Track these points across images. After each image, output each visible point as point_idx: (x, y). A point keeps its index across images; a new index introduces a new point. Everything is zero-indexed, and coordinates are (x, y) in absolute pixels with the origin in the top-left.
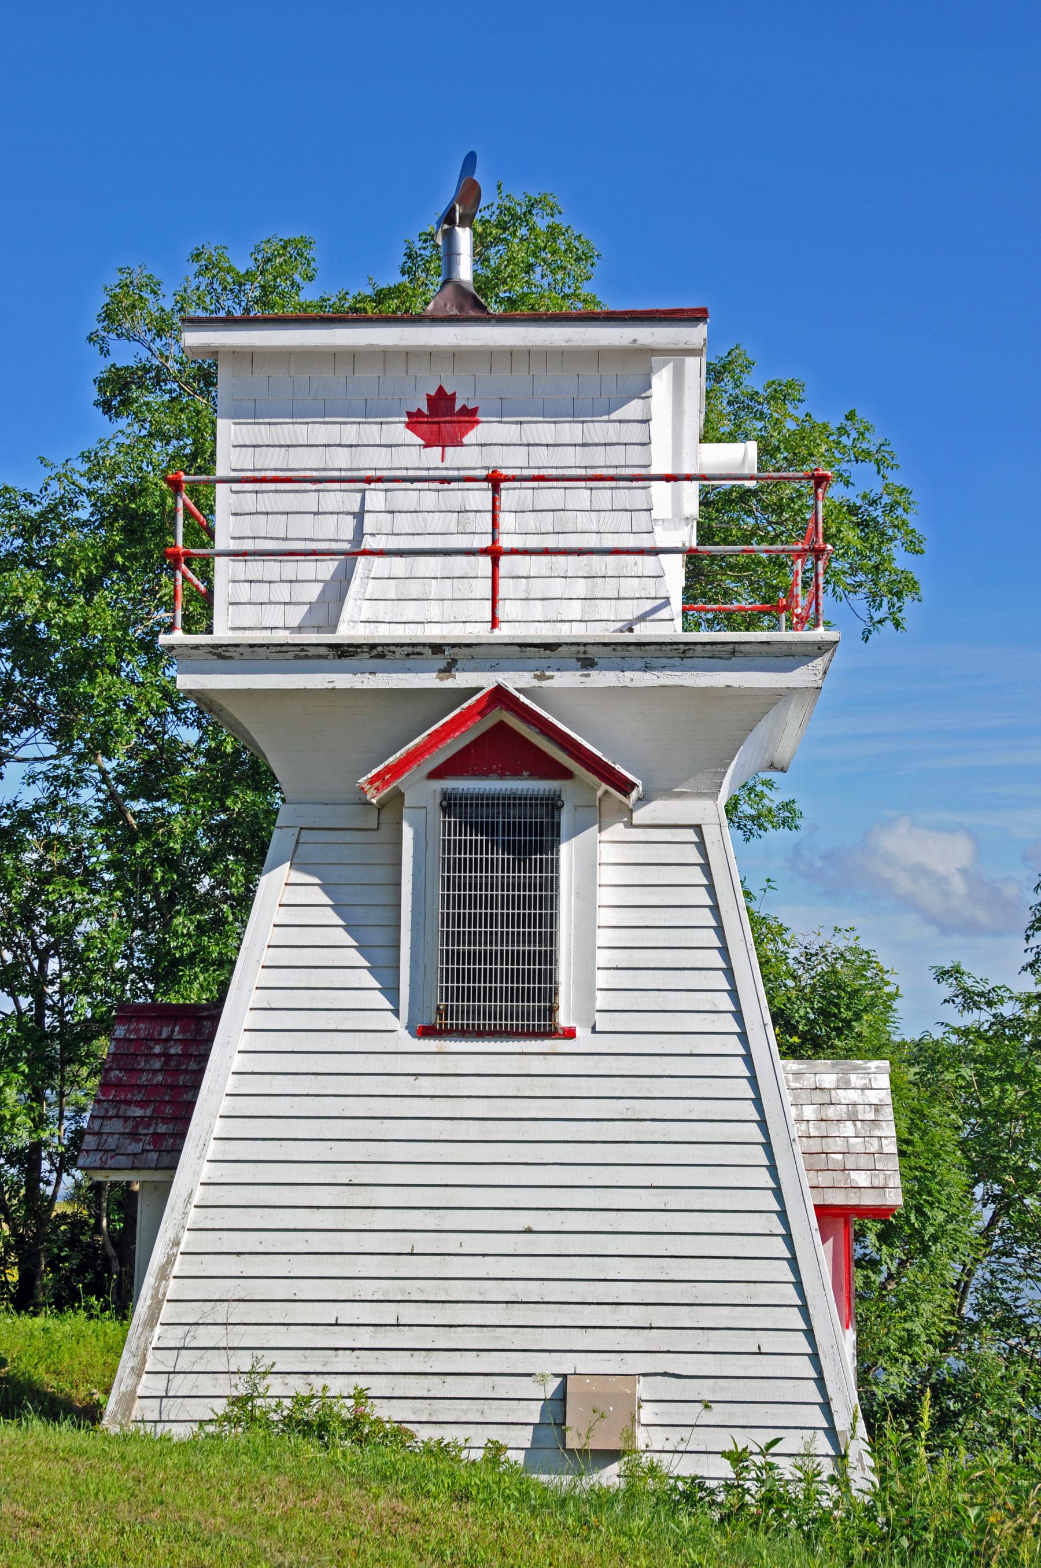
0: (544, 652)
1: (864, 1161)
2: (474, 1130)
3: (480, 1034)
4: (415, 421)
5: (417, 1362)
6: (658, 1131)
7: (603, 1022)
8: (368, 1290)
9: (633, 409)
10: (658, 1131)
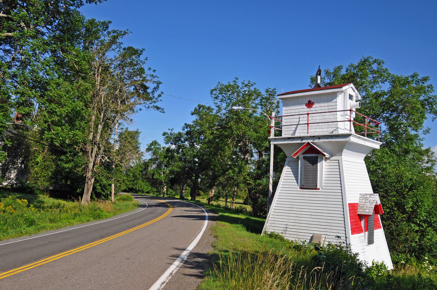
1: (368, 208)
4: (306, 105)
5: (296, 230)
7: (323, 188)
8: (292, 221)
9: (334, 100)
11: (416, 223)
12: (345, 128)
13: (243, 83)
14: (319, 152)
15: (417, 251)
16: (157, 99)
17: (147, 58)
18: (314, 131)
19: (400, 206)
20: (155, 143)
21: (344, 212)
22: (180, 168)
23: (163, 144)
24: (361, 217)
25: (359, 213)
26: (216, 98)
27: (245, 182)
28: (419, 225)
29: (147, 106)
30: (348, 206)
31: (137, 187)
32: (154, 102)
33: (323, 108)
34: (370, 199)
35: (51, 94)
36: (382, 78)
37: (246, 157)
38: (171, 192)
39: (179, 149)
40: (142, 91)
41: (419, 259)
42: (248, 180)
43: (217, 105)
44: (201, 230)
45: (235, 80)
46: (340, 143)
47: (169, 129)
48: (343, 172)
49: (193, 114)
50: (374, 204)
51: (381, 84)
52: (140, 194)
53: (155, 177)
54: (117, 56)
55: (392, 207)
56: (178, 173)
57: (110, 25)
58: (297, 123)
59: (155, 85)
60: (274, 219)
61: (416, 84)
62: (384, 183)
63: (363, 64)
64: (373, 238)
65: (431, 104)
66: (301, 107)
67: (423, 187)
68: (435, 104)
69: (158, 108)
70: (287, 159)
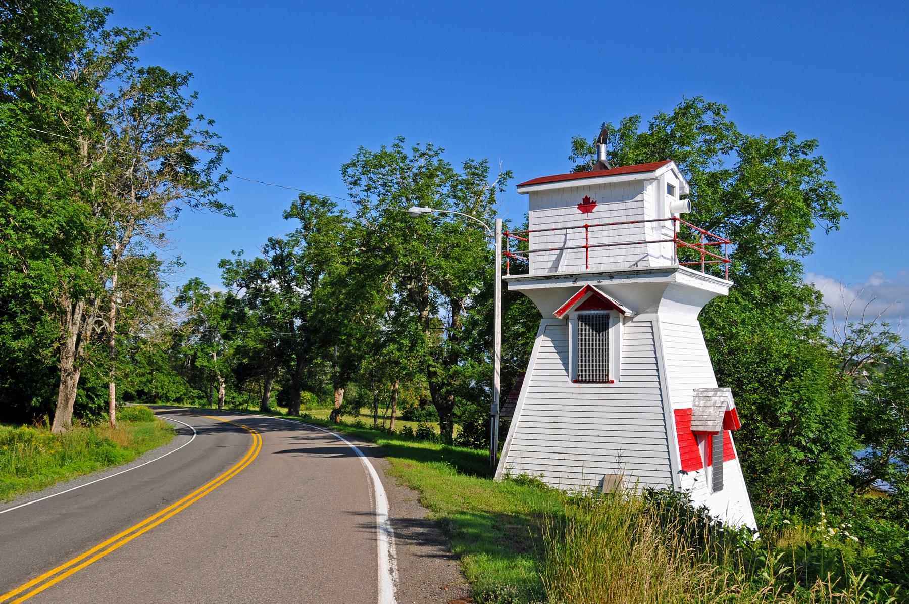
0: (599, 275)
1: (713, 418)
2: (586, 409)
3: (589, 382)
4: (580, 207)
6: (634, 409)
7: (622, 379)
8: (557, 450)
9: (639, 197)
10: (634, 409)
11: (798, 445)
12: (662, 255)
13: (416, 150)
14: (610, 306)
15: (802, 502)
16: (216, 186)
17: (196, 93)
18: (601, 261)
19: (768, 412)
20: (196, 284)
21: (665, 427)
22: (262, 341)
23: (216, 286)
24: (698, 436)
25: (694, 429)
26: (355, 183)
27: (423, 367)
28: (804, 449)
29: (194, 202)
30: (673, 415)
31: (152, 388)
32: (212, 193)
33: (615, 213)
34: (714, 399)
35: (22, 188)
36: (724, 142)
37: (425, 313)
38: (234, 398)
39: (255, 297)
40: (182, 169)
41: (809, 517)
42: (430, 365)
43: (358, 199)
44: (371, 479)
45: (397, 142)
46: (653, 287)
47: (233, 253)
48: (661, 345)
49: (287, 216)
50: (724, 409)
51: (721, 156)
52: (160, 404)
53: (198, 364)
54: (126, 87)
55: (752, 414)
56: (257, 352)
57: (108, 19)
58: (561, 245)
59: (213, 155)
60: (520, 448)
61: (790, 154)
62: (734, 366)
63: (684, 114)
64: (722, 478)
65: (823, 199)
66: (568, 210)
67: (813, 372)
68: (830, 199)
69: (219, 206)
70: (542, 322)
